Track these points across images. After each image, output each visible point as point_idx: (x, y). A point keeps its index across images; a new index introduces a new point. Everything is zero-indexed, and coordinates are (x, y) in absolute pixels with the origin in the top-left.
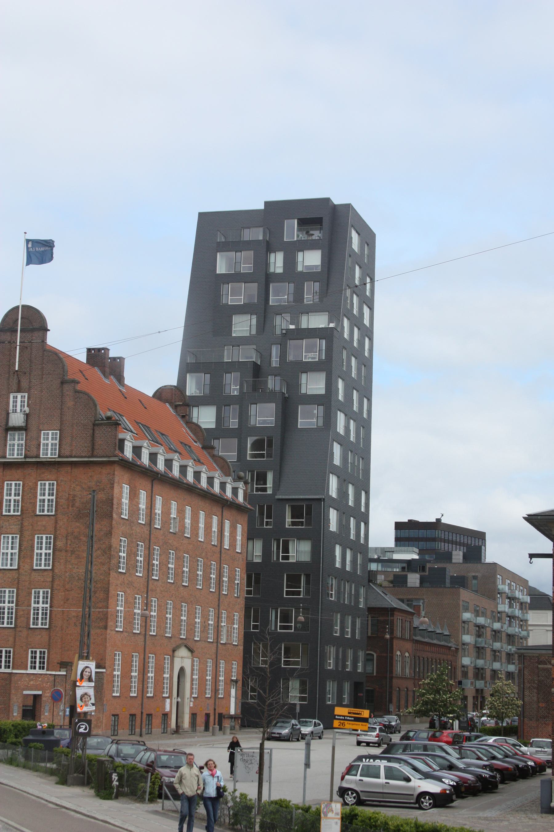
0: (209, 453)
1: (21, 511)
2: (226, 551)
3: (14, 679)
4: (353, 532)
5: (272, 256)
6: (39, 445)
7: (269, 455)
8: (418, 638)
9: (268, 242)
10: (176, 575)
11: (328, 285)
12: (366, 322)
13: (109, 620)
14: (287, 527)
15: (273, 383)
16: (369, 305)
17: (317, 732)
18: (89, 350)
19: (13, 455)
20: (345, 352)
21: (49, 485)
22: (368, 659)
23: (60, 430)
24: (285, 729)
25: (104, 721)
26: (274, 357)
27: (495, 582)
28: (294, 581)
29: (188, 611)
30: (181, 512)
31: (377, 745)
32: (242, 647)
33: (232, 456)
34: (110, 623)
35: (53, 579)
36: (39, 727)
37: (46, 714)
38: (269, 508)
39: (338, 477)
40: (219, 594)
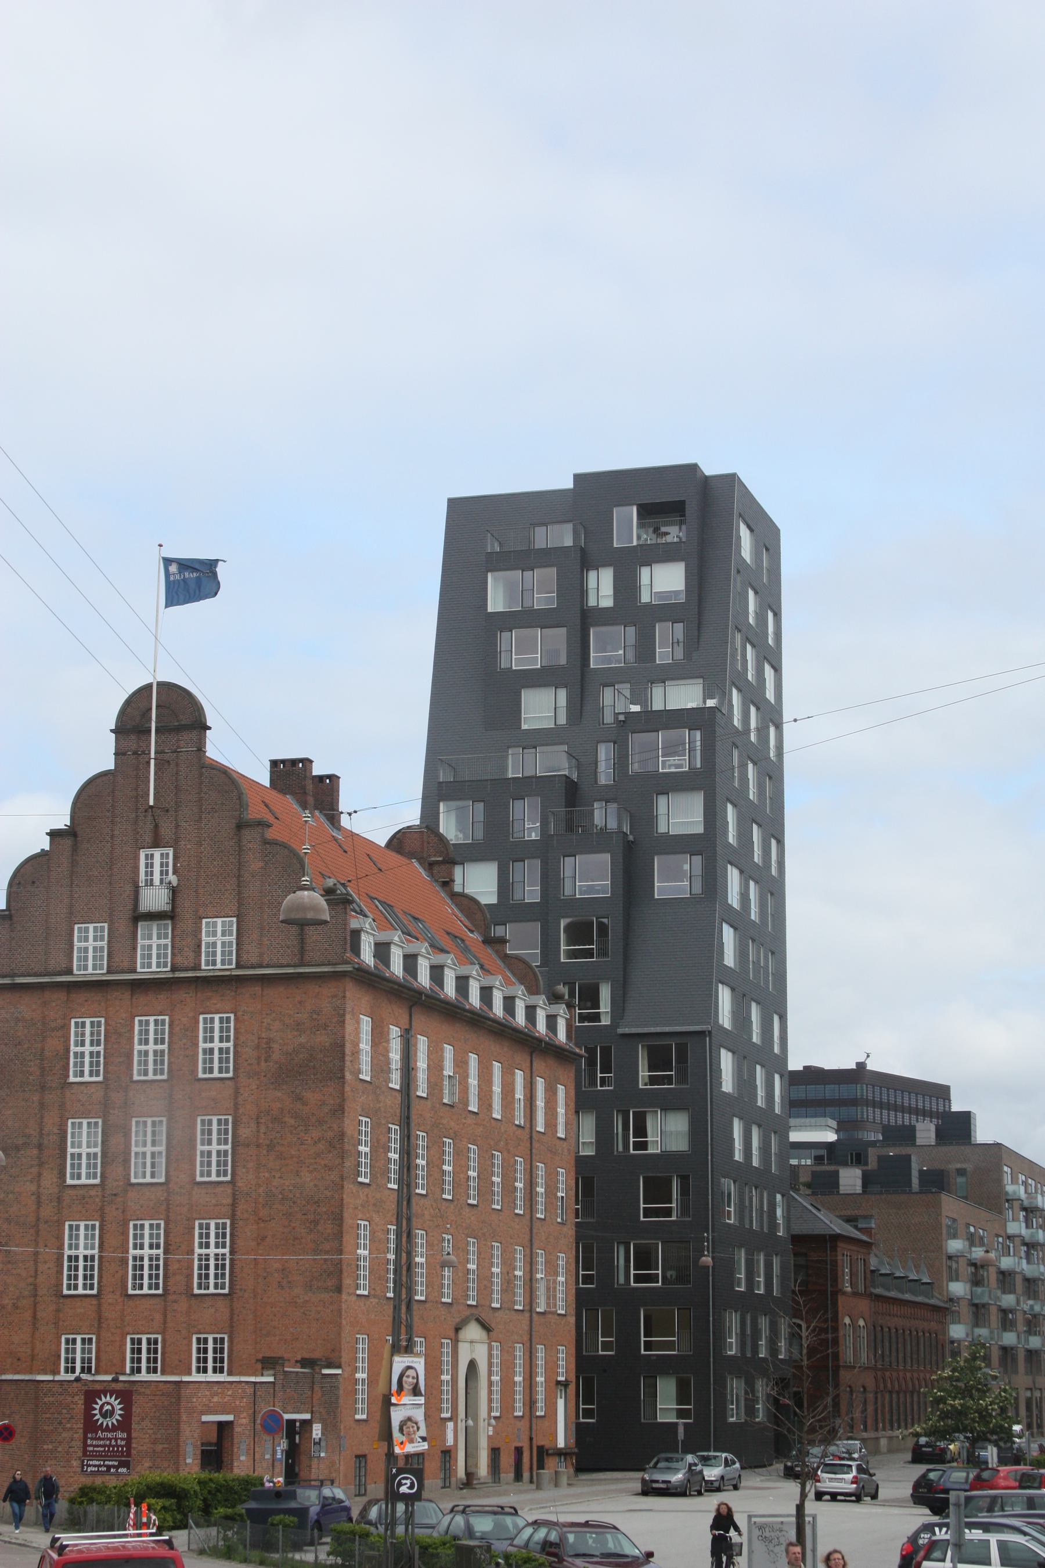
0: (497, 952)
1: (169, 1072)
2: (541, 1136)
3: (185, 1392)
4: (761, 1093)
5: (592, 575)
6: (199, 946)
7: (603, 952)
8: (879, 1291)
9: (582, 550)
10: (456, 1185)
11: (699, 630)
12: (770, 695)
13: (345, 1274)
15: (604, 816)
17: (731, 1476)
18: (274, 763)
19: (150, 966)
20: (736, 753)
21: (221, 1022)
22: (794, 1336)
23: (238, 916)
24: (675, 1474)
25: (342, 1468)
27: (999, 1181)
28: (658, 1190)
29: (479, 1253)
30: (461, 1064)
31: (853, 1498)
32: (574, 1318)
33: (532, 953)
34: (347, 1281)
35: (234, 1200)
36: (267, 1485)
37: (243, 1458)
38: (606, 1052)
39: (733, 989)
40: (531, 1218)
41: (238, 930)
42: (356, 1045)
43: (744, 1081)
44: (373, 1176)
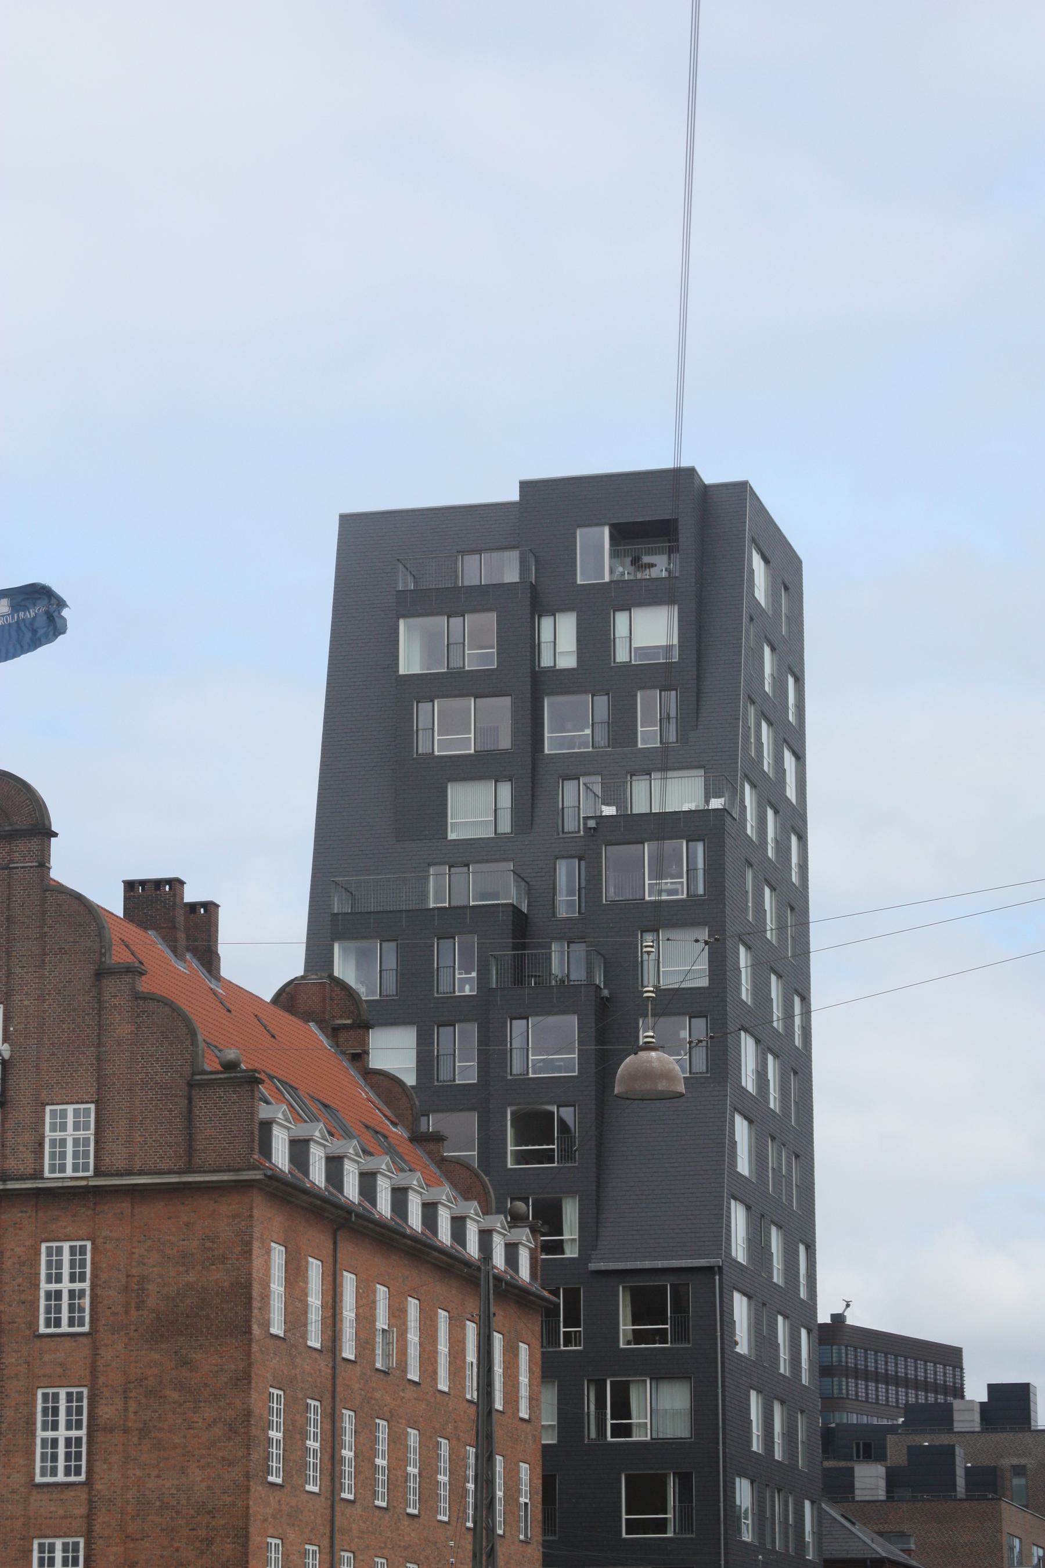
0: (430, 1154)
4: (784, 1355)
6: (41, 1145)
9: (533, 588)
12: (791, 793)
14: (622, 1346)
15: (563, 961)
16: (796, 749)
18: (130, 886)
20: (749, 875)
23: (97, 1103)
26: (564, 892)
30: (398, 1313)
35: (90, 1510)
38: (572, 1296)
39: (748, 1208)
41: (97, 1122)
42: (266, 1286)
43: (763, 1338)
44: (287, 1475)
